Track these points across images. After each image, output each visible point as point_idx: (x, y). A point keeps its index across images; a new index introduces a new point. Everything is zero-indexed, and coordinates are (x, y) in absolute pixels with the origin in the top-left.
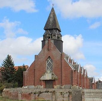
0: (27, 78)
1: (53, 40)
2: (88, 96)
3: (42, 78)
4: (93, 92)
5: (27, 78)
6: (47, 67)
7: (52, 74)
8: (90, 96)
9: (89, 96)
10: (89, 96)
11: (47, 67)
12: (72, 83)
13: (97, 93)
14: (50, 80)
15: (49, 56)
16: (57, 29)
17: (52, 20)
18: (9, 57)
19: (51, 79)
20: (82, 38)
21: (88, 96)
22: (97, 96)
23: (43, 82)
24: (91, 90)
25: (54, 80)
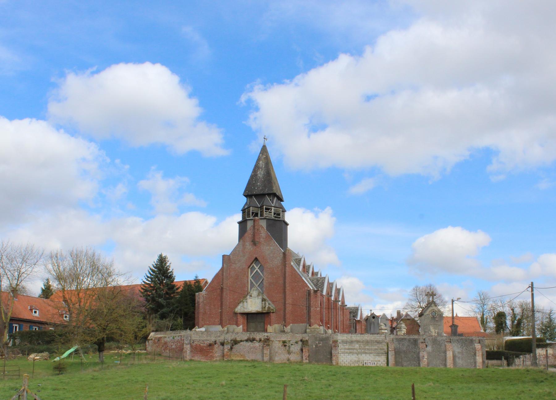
1: (265, 221)
2: (345, 349)
3: (240, 309)
4: (358, 342)
7: (263, 300)
8: (352, 349)
9: (349, 349)
10: (349, 349)
12: (309, 318)
13: (367, 342)
16: (275, 195)
18: (162, 260)
22: (368, 349)
23: (241, 319)
24: (354, 337)
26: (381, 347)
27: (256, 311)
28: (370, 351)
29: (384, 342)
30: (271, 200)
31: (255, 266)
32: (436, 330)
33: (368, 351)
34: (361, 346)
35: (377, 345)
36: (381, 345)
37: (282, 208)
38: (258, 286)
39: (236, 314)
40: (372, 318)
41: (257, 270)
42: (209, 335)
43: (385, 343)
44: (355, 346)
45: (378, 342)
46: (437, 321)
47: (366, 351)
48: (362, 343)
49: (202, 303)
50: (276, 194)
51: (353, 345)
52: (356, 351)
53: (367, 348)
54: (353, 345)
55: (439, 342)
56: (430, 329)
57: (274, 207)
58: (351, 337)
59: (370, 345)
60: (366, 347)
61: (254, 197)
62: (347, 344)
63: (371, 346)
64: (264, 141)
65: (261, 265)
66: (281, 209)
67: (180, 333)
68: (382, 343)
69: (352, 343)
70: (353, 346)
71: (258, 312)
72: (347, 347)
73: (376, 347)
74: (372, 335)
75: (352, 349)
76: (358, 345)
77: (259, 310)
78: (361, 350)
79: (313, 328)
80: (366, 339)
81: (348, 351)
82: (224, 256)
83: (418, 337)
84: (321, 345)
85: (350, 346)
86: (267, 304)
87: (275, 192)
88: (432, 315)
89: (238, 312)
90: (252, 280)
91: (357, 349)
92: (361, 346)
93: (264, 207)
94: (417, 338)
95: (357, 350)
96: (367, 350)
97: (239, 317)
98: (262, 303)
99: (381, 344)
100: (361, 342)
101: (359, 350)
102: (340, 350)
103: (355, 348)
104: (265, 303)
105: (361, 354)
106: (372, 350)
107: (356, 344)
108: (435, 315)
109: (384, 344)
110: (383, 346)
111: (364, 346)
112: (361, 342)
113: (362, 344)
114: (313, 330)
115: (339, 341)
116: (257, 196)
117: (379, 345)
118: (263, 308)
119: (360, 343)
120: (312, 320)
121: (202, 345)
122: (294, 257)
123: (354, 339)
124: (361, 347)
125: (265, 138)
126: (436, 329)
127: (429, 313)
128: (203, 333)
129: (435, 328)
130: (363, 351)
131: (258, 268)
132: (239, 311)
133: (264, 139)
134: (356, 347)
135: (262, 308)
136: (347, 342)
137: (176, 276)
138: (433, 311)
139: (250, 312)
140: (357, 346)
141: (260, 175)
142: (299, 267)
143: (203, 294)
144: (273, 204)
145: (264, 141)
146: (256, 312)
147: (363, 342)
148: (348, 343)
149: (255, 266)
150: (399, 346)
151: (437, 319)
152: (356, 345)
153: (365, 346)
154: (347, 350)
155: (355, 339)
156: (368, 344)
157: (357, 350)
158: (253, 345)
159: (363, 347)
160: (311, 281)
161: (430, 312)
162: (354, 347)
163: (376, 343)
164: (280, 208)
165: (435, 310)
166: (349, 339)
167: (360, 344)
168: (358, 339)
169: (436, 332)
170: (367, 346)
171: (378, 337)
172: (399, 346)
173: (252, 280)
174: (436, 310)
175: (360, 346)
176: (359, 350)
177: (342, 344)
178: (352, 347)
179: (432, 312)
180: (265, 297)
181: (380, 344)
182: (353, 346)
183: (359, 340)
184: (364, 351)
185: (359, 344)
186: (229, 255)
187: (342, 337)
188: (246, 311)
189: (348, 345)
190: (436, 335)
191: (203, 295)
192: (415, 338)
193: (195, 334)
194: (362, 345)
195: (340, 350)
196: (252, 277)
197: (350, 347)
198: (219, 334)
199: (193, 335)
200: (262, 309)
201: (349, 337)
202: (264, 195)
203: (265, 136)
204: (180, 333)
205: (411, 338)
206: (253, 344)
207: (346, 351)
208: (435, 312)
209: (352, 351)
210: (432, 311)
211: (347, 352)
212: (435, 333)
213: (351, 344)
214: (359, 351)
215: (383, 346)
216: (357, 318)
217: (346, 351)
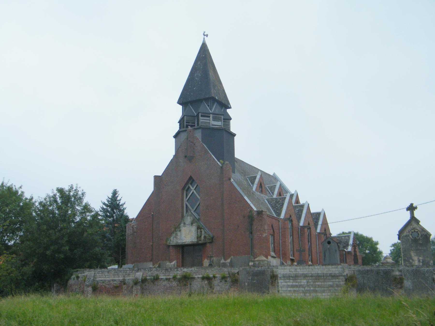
0: (303, 282)
1: (200, 131)
2: (288, 286)
3: (173, 241)
4: (305, 276)
5: (303, 282)
6: (186, 205)
7: (199, 228)
8: (297, 286)
9: (292, 286)
10: (292, 286)
11: (186, 205)
12: (252, 247)
13: (318, 277)
14: (192, 246)
15: (191, 178)
16: (212, 100)
17: (200, 75)
18: (115, 193)
19: (195, 240)
20: (404, 286)
21: (288, 286)
22: (319, 286)
23: (172, 251)
24: (301, 270)
25: (204, 244)
26: (337, 283)
27: (191, 242)
28: (323, 289)
29: (342, 276)
30: (208, 106)
31: (190, 186)
32: (421, 258)
33: (319, 289)
34: (310, 282)
35: (331, 280)
36: (337, 280)
37: (223, 115)
38: (195, 211)
39: (169, 246)
40: (327, 243)
41: (193, 192)
42: (116, 274)
43: (343, 277)
44: (301, 282)
45: (334, 276)
46: (421, 244)
47: (317, 289)
48: (310, 278)
49: (132, 236)
50: (216, 99)
51: (299, 281)
52: (303, 289)
53: (319, 285)
54: (299, 281)
55: (424, 274)
56: (411, 256)
57: (213, 114)
58: (296, 269)
59: (321, 280)
60: (317, 283)
61: (191, 105)
62: (290, 279)
63: (324, 282)
64: (204, 38)
65: (197, 185)
66: (222, 117)
67: (84, 273)
68: (339, 278)
69: (297, 278)
70: (298, 282)
71: (193, 243)
72: (291, 284)
73: (331, 283)
74: (324, 267)
75: (297, 286)
76: (305, 281)
77: (193, 241)
78: (310, 288)
79: (258, 261)
80: (316, 272)
81: (292, 289)
82: (156, 177)
83: (391, 268)
84: (255, 281)
85: (294, 282)
86: (203, 232)
87: (213, 95)
88: (412, 237)
89: (170, 244)
90: (188, 204)
91: (304, 286)
92: (310, 282)
93: (200, 114)
94: (389, 269)
95: (304, 288)
96: (318, 287)
97: (171, 251)
98: (197, 232)
99: (338, 279)
100: (309, 276)
101: (307, 288)
102: (281, 287)
103: (301, 285)
104: (201, 232)
105: (310, 293)
106: (324, 287)
107: (303, 279)
108: (418, 236)
109: (341, 279)
110: (340, 281)
111: (314, 282)
112: (309, 276)
113: (310, 279)
114: (257, 263)
115: (279, 276)
116: (192, 103)
117: (335, 280)
118: (199, 237)
119: (308, 278)
120: (256, 250)
121: (108, 286)
122: (249, 175)
123: (299, 273)
124: (309, 283)
125: (205, 34)
126: (420, 256)
127: (408, 234)
128: (110, 271)
129: (418, 255)
130: (312, 288)
131: (195, 189)
132: (172, 243)
133: (203, 36)
134: (302, 283)
135: (198, 238)
136: (289, 277)
137: (391, 245)
138: (415, 231)
139: (184, 244)
140: (304, 283)
141: (197, 78)
142: (253, 186)
143: (133, 224)
144: (211, 110)
145: (204, 38)
146: (190, 243)
147: (311, 276)
148: (291, 278)
149: (190, 186)
150: (364, 281)
151: (421, 242)
152: (302, 281)
153: (316, 282)
154: (290, 288)
155: (301, 273)
156: (319, 279)
157: (304, 288)
158: (169, 284)
159: (312, 283)
160: (268, 203)
161: (409, 232)
162: (299, 284)
163: (330, 278)
164: (221, 115)
165: (417, 229)
166: (293, 273)
167: (309, 280)
168: (305, 273)
169: (421, 261)
170: (317, 282)
171: (334, 270)
172: (364, 281)
173: (188, 204)
174: (418, 228)
175: (308, 282)
176: (307, 288)
177: (284, 280)
178: (297, 284)
179: (412, 232)
180: (202, 224)
181: (335, 279)
182: (298, 282)
183: (307, 274)
184: (314, 289)
185: (306, 280)
186: (161, 175)
187: (283, 270)
188: (180, 242)
189: (291, 281)
190: (421, 264)
191: (133, 226)
192: (385, 270)
193: (100, 272)
194: (310, 281)
195: (281, 287)
196: (187, 201)
197: (294, 284)
198: (128, 272)
199: (97, 275)
200: (197, 239)
201: (293, 270)
202: (200, 101)
203: (205, 32)
204: (84, 273)
205: (380, 269)
206: (170, 283)
207: (289, 289)
208: (417, 232)
209: (297, 289)
210: (413, 231)
211: (290, 291)
212: (419, 261)
213: (296, 279)
214: (306, 288)
215: (340, 281)
216: (347, 249)
217: (289, 289)
